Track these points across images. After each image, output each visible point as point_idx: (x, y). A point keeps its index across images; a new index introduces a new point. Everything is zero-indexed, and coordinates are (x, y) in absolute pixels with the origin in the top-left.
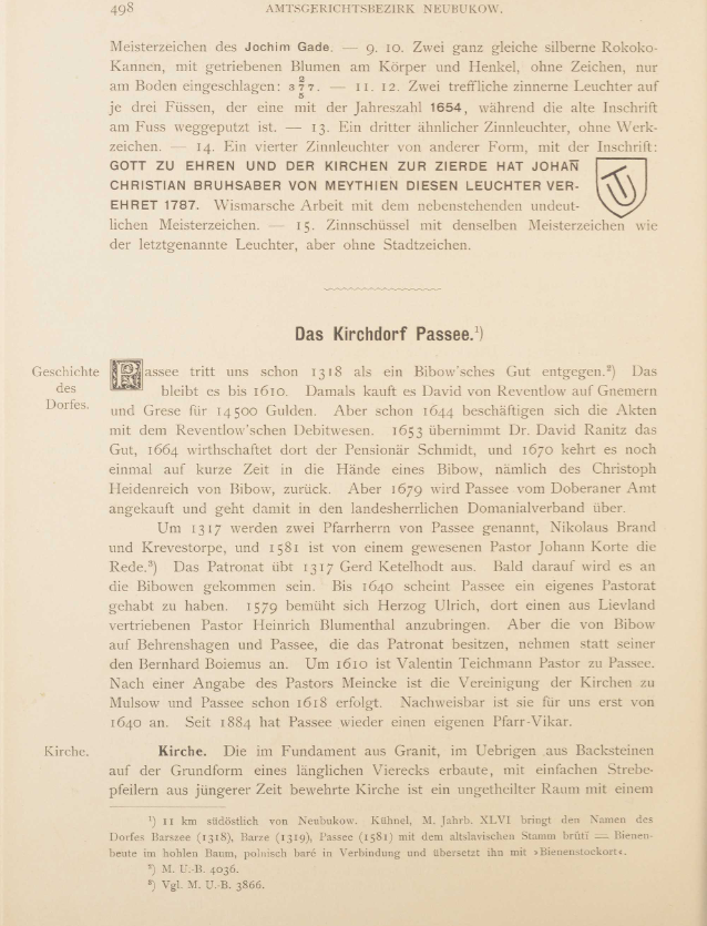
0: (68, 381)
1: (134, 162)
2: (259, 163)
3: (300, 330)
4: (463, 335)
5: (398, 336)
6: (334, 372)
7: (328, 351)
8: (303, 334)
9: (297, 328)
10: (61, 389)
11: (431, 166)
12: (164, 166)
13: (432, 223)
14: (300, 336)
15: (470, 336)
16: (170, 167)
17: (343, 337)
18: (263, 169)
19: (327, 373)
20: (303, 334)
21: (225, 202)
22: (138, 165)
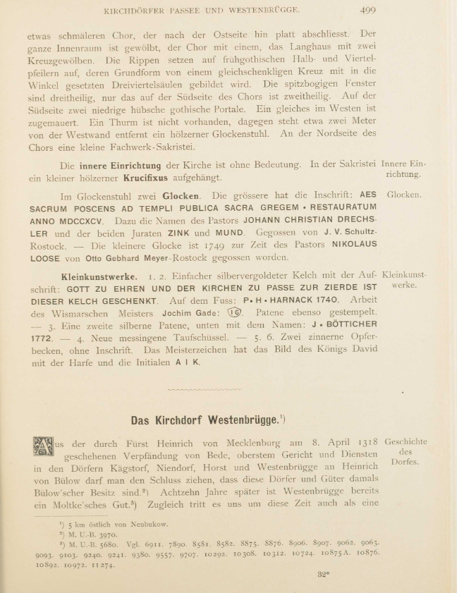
0: (407, 447)
1: (82, 287)
2: (160, 287)
3: (134, 418)
4: (273, 420)
5: (196, 422)
6: (372, 442)
7: (152, 433)
8: (135, 421)
9: (132, 417)
10: (403, 452)
11: (322, 287)
12: (100, 289)
13: (234, 323)
14: (134, 422)
15: (277, 421)
16: (104, 290)
17: (162, 422)
18: (163, 290)
19: (368, 443)
20: (135, 421)
21: (59, 312)
22: (84, 289)
